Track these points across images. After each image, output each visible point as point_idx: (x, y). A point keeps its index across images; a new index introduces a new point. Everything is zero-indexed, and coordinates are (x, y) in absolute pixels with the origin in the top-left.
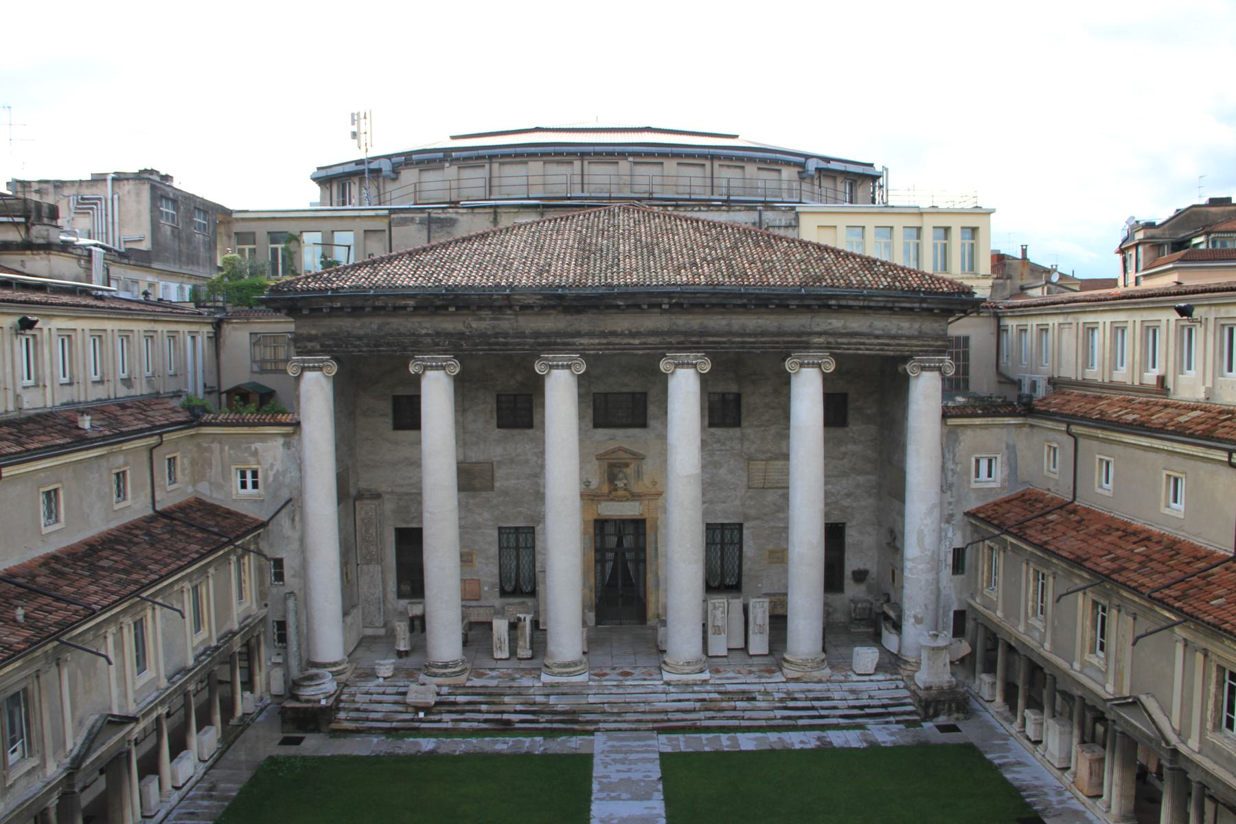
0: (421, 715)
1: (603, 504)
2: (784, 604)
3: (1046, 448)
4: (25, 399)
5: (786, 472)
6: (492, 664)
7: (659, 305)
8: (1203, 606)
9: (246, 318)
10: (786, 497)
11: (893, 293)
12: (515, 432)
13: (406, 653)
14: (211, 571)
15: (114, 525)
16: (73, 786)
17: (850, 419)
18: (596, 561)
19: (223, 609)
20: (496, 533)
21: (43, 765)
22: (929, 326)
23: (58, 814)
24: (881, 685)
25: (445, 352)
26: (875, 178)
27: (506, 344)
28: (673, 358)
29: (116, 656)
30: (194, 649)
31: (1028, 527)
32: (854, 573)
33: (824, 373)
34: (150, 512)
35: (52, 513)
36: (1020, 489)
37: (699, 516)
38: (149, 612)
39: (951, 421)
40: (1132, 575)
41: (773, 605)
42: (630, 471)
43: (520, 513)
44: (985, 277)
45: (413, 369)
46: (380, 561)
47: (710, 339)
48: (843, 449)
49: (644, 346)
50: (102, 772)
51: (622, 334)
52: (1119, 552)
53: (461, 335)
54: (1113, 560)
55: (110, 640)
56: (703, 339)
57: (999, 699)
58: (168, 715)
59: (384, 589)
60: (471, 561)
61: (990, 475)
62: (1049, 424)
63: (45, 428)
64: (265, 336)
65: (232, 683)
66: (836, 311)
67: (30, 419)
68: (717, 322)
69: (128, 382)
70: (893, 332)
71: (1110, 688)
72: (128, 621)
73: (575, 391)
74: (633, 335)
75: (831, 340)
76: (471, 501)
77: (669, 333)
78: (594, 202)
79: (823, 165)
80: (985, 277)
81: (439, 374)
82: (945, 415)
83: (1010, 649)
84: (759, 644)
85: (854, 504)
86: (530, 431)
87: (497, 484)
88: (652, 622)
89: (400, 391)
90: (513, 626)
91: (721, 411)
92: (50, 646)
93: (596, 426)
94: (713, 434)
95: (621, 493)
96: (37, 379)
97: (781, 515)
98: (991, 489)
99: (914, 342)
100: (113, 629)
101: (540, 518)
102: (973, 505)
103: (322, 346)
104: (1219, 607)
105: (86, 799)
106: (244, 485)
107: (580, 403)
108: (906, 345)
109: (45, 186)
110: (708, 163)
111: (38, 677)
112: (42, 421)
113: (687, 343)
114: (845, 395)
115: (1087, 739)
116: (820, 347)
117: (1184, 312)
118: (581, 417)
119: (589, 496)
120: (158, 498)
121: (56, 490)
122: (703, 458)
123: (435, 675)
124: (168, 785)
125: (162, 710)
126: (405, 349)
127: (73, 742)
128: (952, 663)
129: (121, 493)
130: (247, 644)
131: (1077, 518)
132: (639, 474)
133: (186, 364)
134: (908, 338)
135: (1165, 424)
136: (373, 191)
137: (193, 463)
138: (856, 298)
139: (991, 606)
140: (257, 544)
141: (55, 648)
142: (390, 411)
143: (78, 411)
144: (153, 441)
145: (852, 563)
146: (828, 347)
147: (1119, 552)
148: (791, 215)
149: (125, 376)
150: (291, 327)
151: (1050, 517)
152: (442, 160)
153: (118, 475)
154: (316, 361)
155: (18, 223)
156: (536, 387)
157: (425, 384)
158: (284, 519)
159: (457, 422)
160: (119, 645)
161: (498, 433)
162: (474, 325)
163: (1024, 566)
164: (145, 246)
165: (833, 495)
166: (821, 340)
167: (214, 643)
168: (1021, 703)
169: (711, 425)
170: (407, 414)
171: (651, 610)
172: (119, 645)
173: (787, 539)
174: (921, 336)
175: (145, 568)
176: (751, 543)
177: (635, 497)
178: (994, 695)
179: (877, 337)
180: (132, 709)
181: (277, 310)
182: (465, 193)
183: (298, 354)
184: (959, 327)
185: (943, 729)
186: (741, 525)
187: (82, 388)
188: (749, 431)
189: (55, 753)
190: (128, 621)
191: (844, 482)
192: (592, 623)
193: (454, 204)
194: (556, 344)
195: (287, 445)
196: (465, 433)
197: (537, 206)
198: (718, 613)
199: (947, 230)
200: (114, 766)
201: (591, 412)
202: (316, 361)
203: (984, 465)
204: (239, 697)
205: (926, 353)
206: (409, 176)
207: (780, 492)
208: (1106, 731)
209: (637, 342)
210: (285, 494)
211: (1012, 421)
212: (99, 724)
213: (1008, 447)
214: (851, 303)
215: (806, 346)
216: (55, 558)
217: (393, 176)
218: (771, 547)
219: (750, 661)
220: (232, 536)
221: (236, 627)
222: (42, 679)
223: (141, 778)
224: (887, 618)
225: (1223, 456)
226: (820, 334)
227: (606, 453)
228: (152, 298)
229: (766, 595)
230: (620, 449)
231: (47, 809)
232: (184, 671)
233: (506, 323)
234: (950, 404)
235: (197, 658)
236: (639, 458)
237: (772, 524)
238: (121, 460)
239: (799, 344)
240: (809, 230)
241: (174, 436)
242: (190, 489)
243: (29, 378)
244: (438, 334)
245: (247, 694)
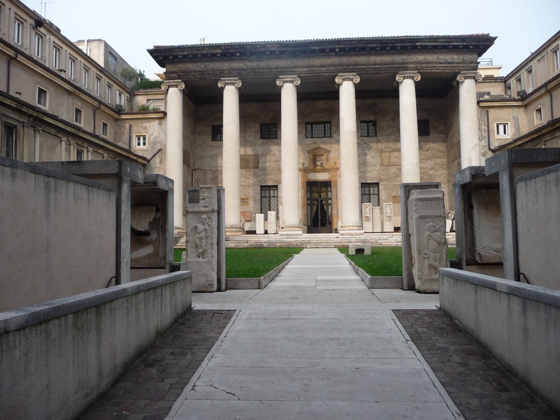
1: (311, 174)
5: (399, 158)
10: (400, 169)
12: (269, 140)
17: (431, 131)
18: (308, 205)
20: (259, 188)
25: (235, 76)
27: (262, 72)
28: (341, 76)
33: (415, 82)
37: (357, 180)
42: (323, 158)
43: (271, 179)
47: (359, 67)
51: (318, 66)
53: (242, 69)
56: (355, 67)
60: (247, 202)
61: (505, 133)
68: (363, 59)
70: (450, 61)
74: (322, 66)
75: (418, 65)
76: (248, 173)
77: (340, 65)
85: (435, 173)
86: (276, 140)
87: (260, 165)
89: (216, 123)
97: (398, 179)
99: (460, 65)
103: (178, 76)
106: (139, 144)
107: (299, 127)
108: (456, 67)
113: (348, 69)
116: (413, 69)
118: (299, 133)
119: (305, 171)
122: (358, 151)
126: (216, 76)
132: (328, 159)
134: (457, 63)
158: (157, 159)
159: (241, 136)
161: (261, 141)
162: (248, 64)
165: (424, 168)
166: (413, 66)
174: (464, 62)
177: (324, 170)
179: (441, 63)
186: (378, 184)
188: (381, 138)
191: (429, 162)
194: (286, 71)
195: (160, 124)
196: (245, 142)
198: (367, 210)
203: (501, 128)
205: (467, 70)
207: (397, 167)
209: (324, 69)
210: (158, 147)
213: (514, 118)
215: (406, 69)
218: (394, 194)
226: (412, 63)
233: (264, 64)
236: (328, 152)
237: (394, 183)
239: (403, 67)
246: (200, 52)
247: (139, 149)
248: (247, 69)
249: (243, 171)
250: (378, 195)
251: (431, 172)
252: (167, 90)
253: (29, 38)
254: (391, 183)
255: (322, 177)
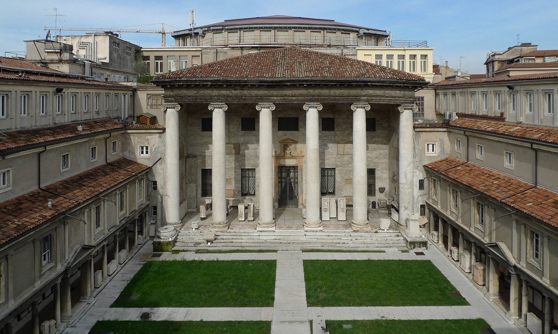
0: (209, 244)
2: (352, 201)
3: (456, 141)
4: (57, 119)
6: (238, 223)
7: (303, 85)
8: (523, 206)
9: (145, 89)
10: (352, 158)
11: (393, 80)
12: (248, 132)
13: (204, 219)
14: (128, 186)
15: (89, 169)
16: (67, 274)
17: (377, 128)
18: (279, 182)
19: (132, 201)
20: (240, 171)
21: (56, 266)
22: (407, 93)
23: (61, 287)
24: (391, 234)
25: (222, 102)
26: (387, 36)
27: (245, 99)
29: (88, 221)
30: (119, 218)
31: (450, 172)
32: (379, 189)
34: (105, 163)
35: (65, 164)
36: (446, 156)
38: (102, 203)
39: (416, 130)
40: (493, 192)
41: (347, 200)
43: (250, 163)
44: (431, 74)
45: (209, 108)
46: (196, 182)
48: (374, 140)
49: (297, 100)
50: (79, 269)
52: (487, 183)
53: (229, 96)
54: (485, 186)
55: (86, 214)
57: (441, 242)
58: (108, 245)
59: (197, 193)
61: (433, 151)
62: (457, 131)
63: (64, 130)
64: (153, 95)
65: (133, 232)
66: (370, 87)
67: (58, 127)
68: (325, 92)
69: (98, 113)
71: (488, 240)
72: (94, 207)
73: (271, 116)
77: (307, 95)
78: (279, 46)
79: (366, 31)
80: (431, 74)
81: (221, 110)
82: (414, 128)
83: (444, 222)
84: (342, 216)
86: (254, 132)
88: (300, 207)
89: (206, 117)
90: (246, 208)
91: (326, 124)
92: (62, 217)
93: (279, 130)
94: (324, 134)
95: (288, 156)
96: (62, 111)
97: (350, 165)
98: (434, 156)
100: (87, 210)
101: (258, 165)
102: (426, 163)
104: (530, 207)
105: (72, 280)
106: (142, 153)
109: (68, 38)
110: (322, 32)
111: (56, 230)
112: (63, 128)
113: (313, 99)
114: (375, 119)
115: (479, 260)
116: (364, 101)
117: (510, 87)
118: (273, 127)
119: (278, 157)
120: (108, 158)
121: (67, 155)
122: (320, 143)
123: (215, 227)
124: (105, 275)
125: (105, 243)
127: (69, 257)
128: (420, 227)
129: (93, 156)
130: (141, 216)
131: (469, 169)
133: (121, 106)
135: (504, 132)
136: (196, 41)
137: (123, 144)
138: (378, 82)
139: (436, 203)
140: (147, 175)
141: (63, 218)
142: (201, 124)
143: (78, 124)
144: (107, 135)
145: (379, 185)
146: (368, 101)
147: (487, 183)
148: (354, 50)
149: (97, 110)
150: (163, 92)
151: (458, 168)
152: (222, 29)
153: (92, 149)
154: (172, 105)
155: (57, 52)
156: (257, 114)
157: (214, 114)
159: (226, 128)
160: (90, 217)
161: (242, 132)
162: (233, 92)
163: (448, 187)
164: (107, 61)
167: (128, 215)
168: (450, 244)
169: (323, 130)
170: (207, 125)
171: (300, 201)
172: (90, 217)
173: (353, 175)
175: (101, 185)
176: (339, 176)
177: (293, 157)
178: (438, 241)
180: (93, 243)
181: (157, 86)
182: (230, 42)
183: (165, 102)
184: (419, 93)
185: (418, 254)
187: (80, 115)
188: (338, 132)
189: (61, 261)
190: (94, 207)
192: (277, 207)
193: (226, 46)
195: (160, 137)
196: (229, 132)
197: (258, 47)
199: (415, 56)
200: (84, 267)
201: (277, 125)
202: (172, 105)
204: (136, 237)
205: (406, 103)
206: (209, 35)
208: (485, 257)
211: (442, 130)
212: (80, 249)
214: (376, 84)
215: (359, 100)
216: (66, 181)
217: (203, 35)
218: (346, 177)
219: (338, 223)
220: (137, 172)
221: (137, 209)
222: (57, 230)
223: (95, 271)
224: (393, 207)
225: (529, 145)
227: (283, 141)
228: (108, 80)
229: (344, 196)
230: (288, 139)
231: (56, 284)
232: (135, 211)
234: (416, 123)
235: (120, 222)
238: (94, 143)
239: (357, 99)
240: (361, 56)
241: (116, 133)
242: (121, 154)
243: (43, 112)
244: (219, 96)
245: (140, 236)
246: (193, 83)
247: (143, 159)
248: (232, 97)
249: (227, 156)
250: (334, 176)
251: (376, 161)
252: (166, 110)
253: (51, 104)
254: (344, 169)
255: (289, 162)
